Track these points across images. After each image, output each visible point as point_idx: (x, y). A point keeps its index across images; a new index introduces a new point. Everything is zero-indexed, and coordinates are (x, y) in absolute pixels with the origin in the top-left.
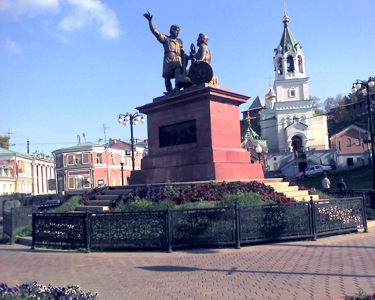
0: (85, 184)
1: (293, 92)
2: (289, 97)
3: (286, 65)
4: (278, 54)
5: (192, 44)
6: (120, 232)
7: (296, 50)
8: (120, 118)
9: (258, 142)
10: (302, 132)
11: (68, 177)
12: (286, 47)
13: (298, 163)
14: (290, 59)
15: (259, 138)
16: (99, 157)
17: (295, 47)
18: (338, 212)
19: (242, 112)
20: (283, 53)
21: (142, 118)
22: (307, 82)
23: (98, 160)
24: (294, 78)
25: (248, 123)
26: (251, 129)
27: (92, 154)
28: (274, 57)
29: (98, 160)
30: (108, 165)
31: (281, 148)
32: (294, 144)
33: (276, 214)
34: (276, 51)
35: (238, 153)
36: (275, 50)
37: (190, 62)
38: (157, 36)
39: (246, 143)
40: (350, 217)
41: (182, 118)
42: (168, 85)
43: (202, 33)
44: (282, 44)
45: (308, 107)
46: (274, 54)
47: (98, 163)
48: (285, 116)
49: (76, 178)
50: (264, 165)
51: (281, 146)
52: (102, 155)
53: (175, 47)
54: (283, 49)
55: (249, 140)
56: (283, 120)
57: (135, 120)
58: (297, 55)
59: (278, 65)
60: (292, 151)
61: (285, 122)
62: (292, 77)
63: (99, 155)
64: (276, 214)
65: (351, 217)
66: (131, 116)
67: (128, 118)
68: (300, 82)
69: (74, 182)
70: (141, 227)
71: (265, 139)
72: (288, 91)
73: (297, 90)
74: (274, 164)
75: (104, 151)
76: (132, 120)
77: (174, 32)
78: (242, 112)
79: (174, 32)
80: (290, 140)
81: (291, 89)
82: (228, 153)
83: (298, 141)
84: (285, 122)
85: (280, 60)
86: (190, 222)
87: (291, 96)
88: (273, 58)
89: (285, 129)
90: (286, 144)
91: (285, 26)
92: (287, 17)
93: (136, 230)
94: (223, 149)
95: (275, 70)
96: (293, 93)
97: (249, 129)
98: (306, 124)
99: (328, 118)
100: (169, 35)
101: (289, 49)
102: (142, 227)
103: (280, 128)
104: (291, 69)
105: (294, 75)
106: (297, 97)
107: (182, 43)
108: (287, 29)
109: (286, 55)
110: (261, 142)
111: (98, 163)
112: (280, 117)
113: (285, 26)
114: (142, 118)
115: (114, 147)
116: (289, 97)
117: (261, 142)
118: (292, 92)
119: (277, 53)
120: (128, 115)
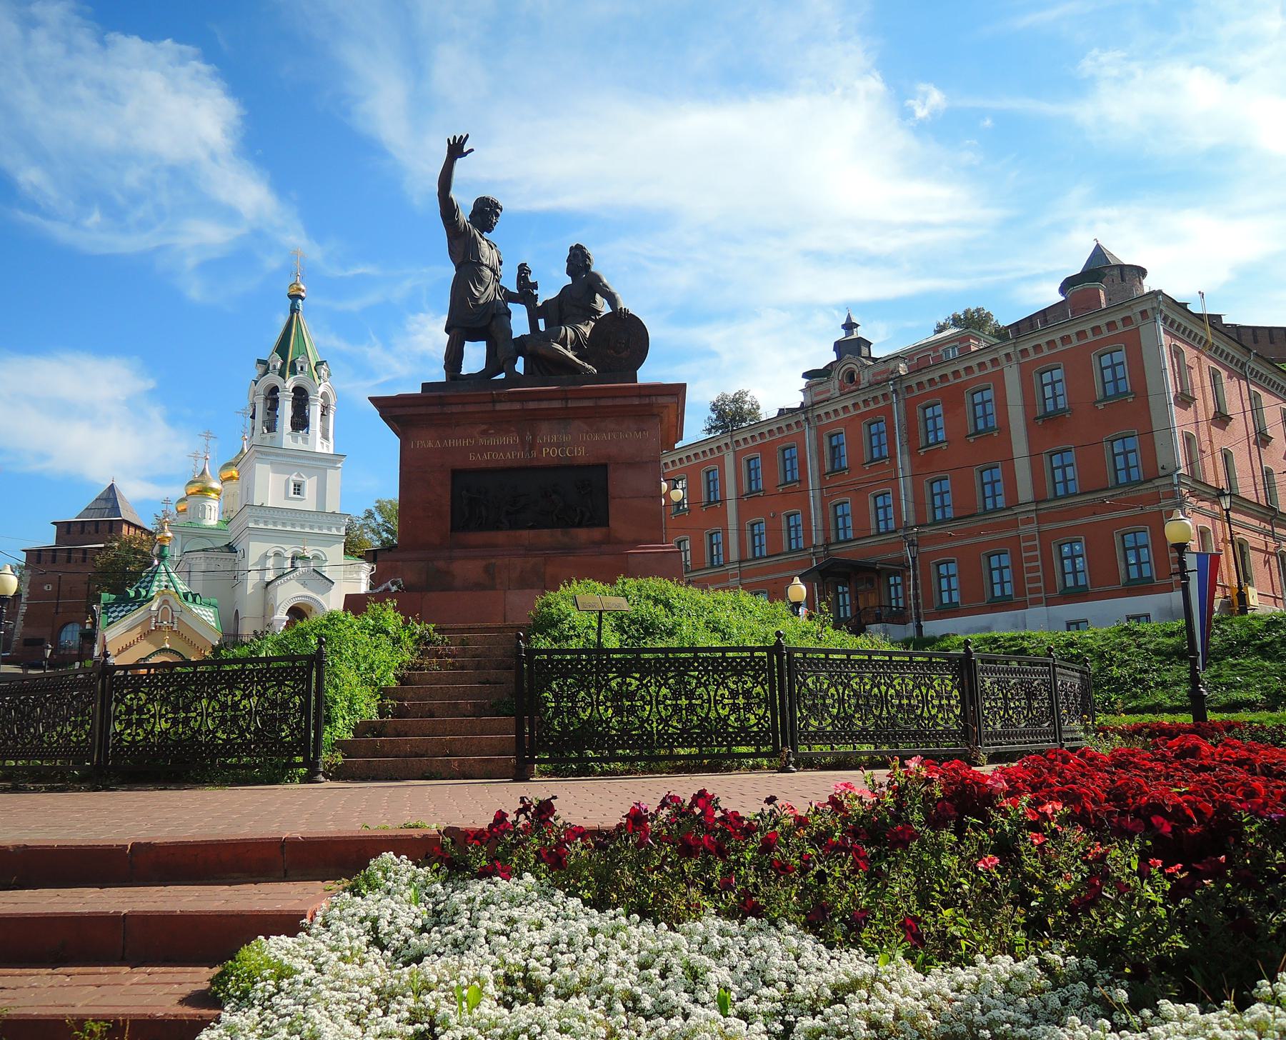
2: (287, 497)
3: (286, 410)
6: (899, 695)
10: (318, 598)
12: (293, 364)
14: (301, 397)
15: (194, 600)
18: (832, 690)
24: (305, 447)
33: (655, 725)
34: (261, 369)
39: (154, 608)
40: (891, 691)
42: (454, 357)
45: (334, 531)
46: (256, 372)
48: (271, 548)
54: (284, 364)
55: (166, 602)
56: (266, 557)
58: (321, 390)
59: (265, 404)
61: (270, 563)
62: (300, 445)
64: (655, 725)
65: (886, 692)
68: (321, 463)
70: (610, 711)
72: (287, 481)
73: (310, 486)
81: (294, 477)
84: (270, 563)
85: (272, 395)
86: (758, 683)
87: (291, 494)
89: (268, 584)
91: (294, 310)
92: (303, 287)
93: (741, 701)
96: (298, 488)
102: (606, 710)
103: (253, 579)
104: (300, 422)
105: (305, 441)
106: (308, 502)
109: (290, 383)
112: (255, 550)
113: (294, 310)
116: (287, 497)
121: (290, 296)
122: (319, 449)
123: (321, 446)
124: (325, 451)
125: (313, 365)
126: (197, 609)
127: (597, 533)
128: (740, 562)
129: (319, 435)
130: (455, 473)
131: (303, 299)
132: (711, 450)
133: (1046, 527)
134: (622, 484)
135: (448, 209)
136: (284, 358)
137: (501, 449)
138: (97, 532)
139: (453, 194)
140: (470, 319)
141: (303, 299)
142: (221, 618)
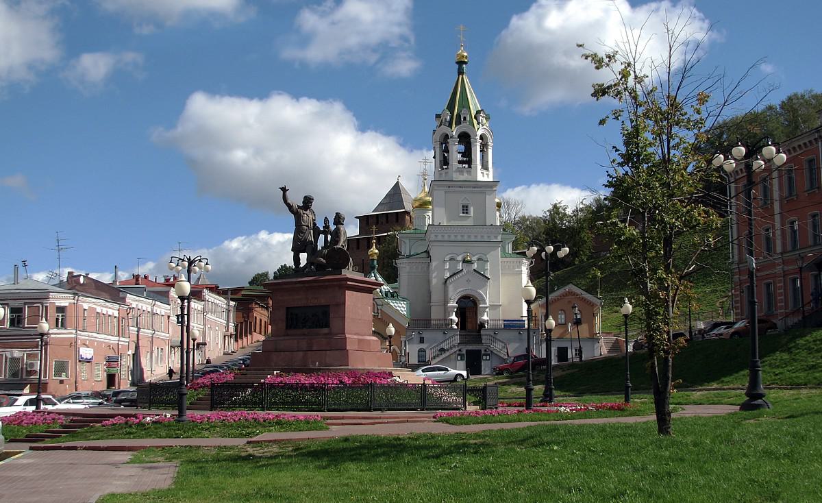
0: (18, 370)
1: (467, 207)
3: (456, 150)
4: (442, 126)
5: (326, 218)
7: (478, 123)
8: (171, 262)
9: (391, 304)
11: (41, 351)
12: (459, 116)
13: (464, 352)
14: (465, 139)
16: (60, 315)
17: (475, 118)
19: (357, 217)
20: (450, 125)
21: (207, 264)
22: (495, 189)
23: (57, 320)
24: (469, 178)
25: (373, 262)
26: (378, 276)
27: (46, 307)
28: (434, 131)
29: (57, 320)
30: (78, 332)
31: (435, 320)
32: (461, 313)
35: (369, 341)
36: (438, 116)
37: (322, 237)
38: (290, 207)
41: (313, 302)
42: (297, 260)
43: (339, 212)
44: (451, 107)
46: (435, 123)
47: (57, 326)
49: (9, 356)
50: (398, 351)
51: (436, 314)
52: (68, 310)
53: (307, 217)
54: (452, 118)
57: (195, 266)
58: (479, 133)
60: (456, 327)
62: (465, 177)
63: (61, 309)
66: (189, 259)
67: (186, 264)
69: (198, 359)
71: (404, 299)
74: (420, 351)
75: (73, 301)
76: (191, 266)
77: (308, 202)
78: (357, 217)
79: (308, 202)
80: (453, 304)
82: (360, 341)
83: (468, 307)
88: (432, 132)
90: (446, 311)
94: (355, 337)
95: (434, 157)
97: (373, 275)
98: (488, 276)
99: (532, 262)
100: (301, 205)
101: (465, 119)
105: (469, 173)
107: (315, 215)
108: (463, 78)
109: (455, 131)
110: (397, 305)
111: (57, 326)
114: (207, 264)
115: (91, 293)
117: (397, 305)
118: (463, 206)
119: (440, 125)
120: (186, 259)
121: (457, 63)
122: (480, 178)
123: (482, 176)
124: (486, 179)
125: (473, 113)
126: (392, 303)
127: (325, 330)
128: (782, 254)
129: (479, 167)
130: (287, 308)
131: (466, 63)
132: (805, 144)
133: (786, 268)
134: (283, 325)
135: (290, 207)
136: (452, 113)
137: (298, 300)
138: (358, 248)
139: (289, 201)
140: (299, 246)
141: (466, 63)
142: (411, 309)
